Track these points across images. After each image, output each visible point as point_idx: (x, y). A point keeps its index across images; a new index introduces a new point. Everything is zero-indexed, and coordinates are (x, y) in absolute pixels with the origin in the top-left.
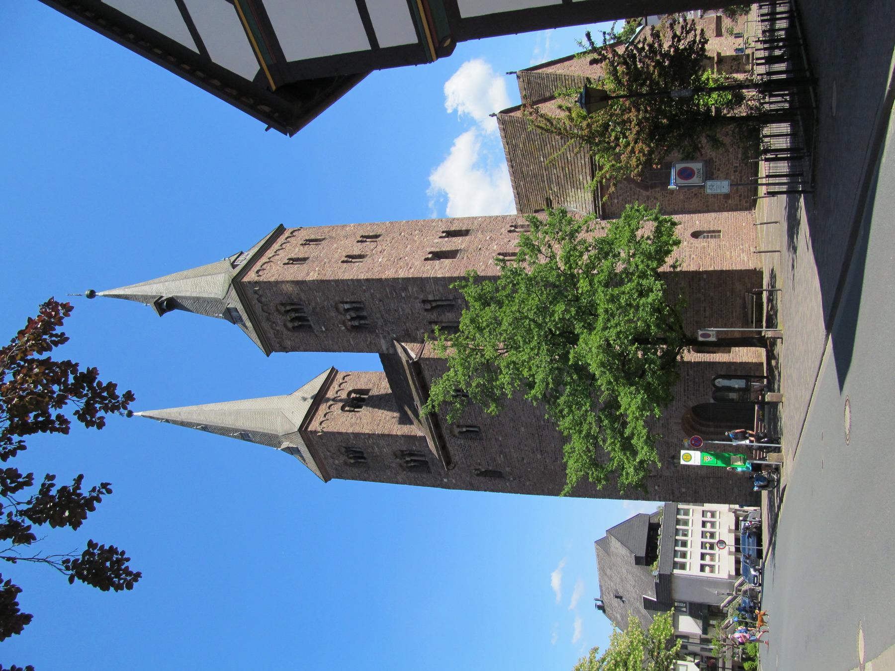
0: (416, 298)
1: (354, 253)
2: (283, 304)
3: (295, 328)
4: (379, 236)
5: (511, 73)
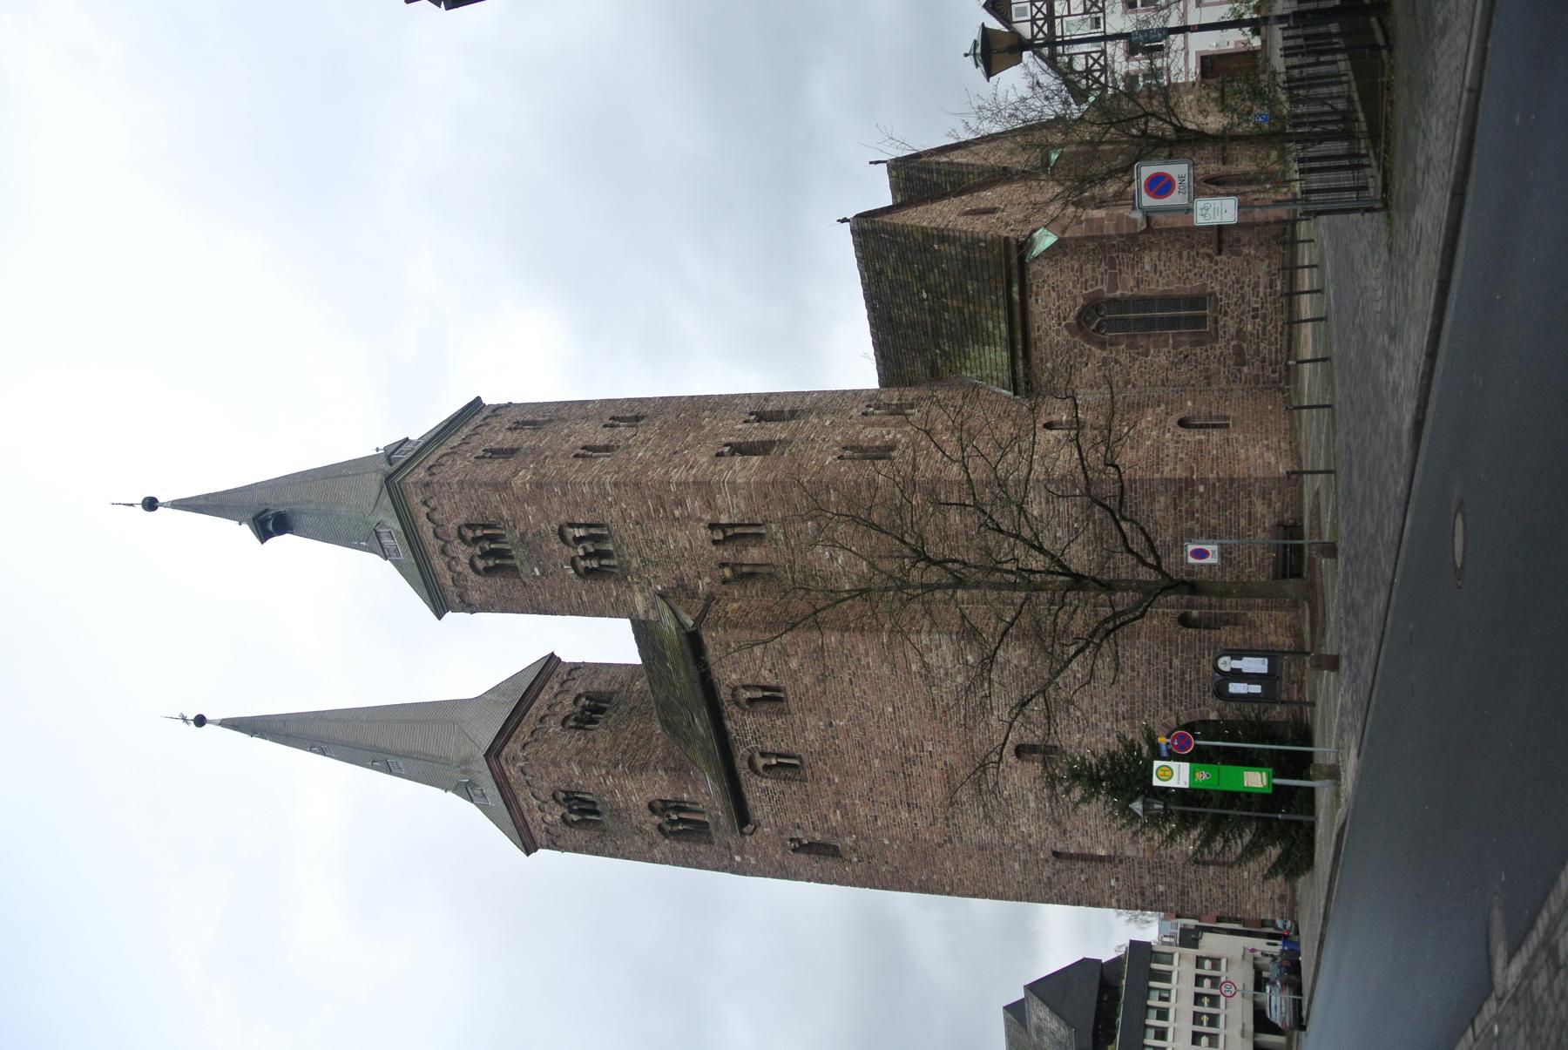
2: (469, 526)
3: (488, 571)
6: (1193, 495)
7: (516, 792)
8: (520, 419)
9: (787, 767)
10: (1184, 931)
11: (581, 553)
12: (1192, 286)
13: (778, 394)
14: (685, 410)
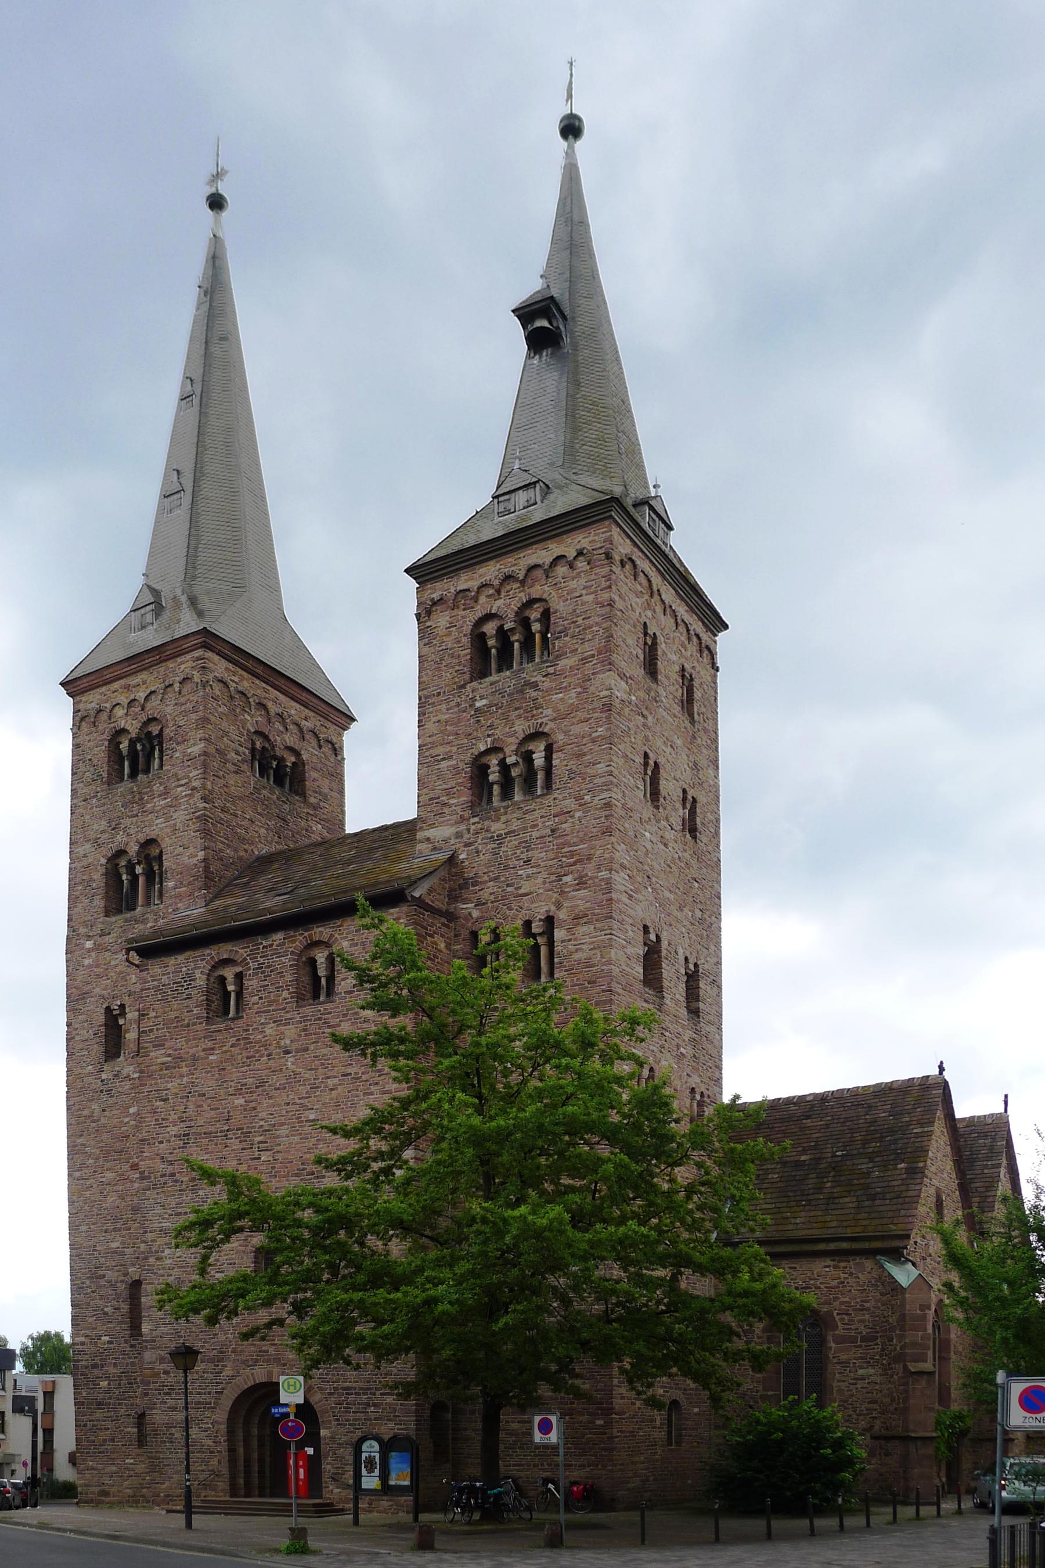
1: (662, 782)
4: (695, 838)
5: (1006, 1103)
6: (591, 1414)
9: (223, 1001)
10: (33, 1399)
11: (510, 760)
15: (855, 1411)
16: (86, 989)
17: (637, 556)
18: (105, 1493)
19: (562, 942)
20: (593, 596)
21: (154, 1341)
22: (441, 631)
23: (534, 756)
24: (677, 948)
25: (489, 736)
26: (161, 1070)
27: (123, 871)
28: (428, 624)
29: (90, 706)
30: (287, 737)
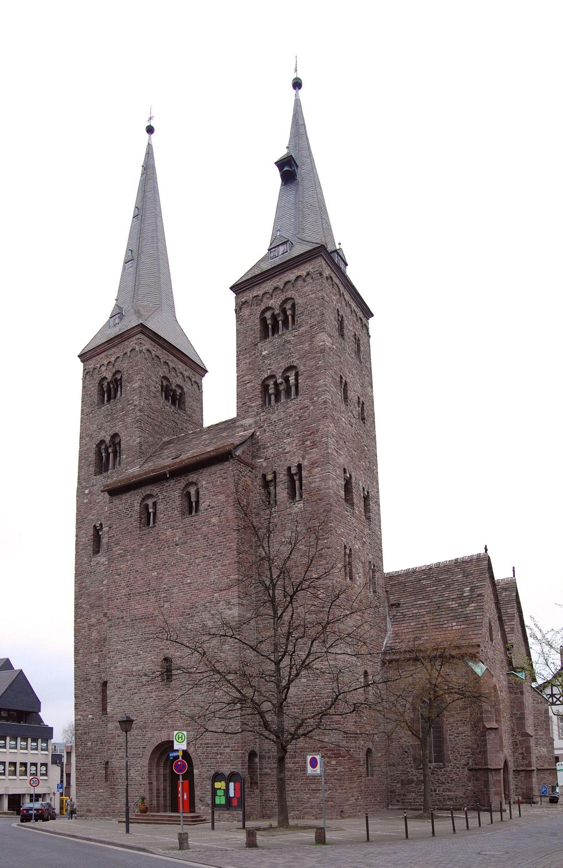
0: (304, 458)
1: (349, 392)
7: (119, 346)
8: (361, 342)
9: (147, 517)
10: (61, 756)
12: (449, 754)
13: (379, 510)
14: (369, 450)
15: (459, 753)
16: (85, 515)
17: (333, 275)
18: (89, 811)
19: (306, 478)
20: (314, 295)
21: (113, 717)
22: (246, 317)
23: (290, 378)
24: (360, 482)
25: (269, 369)
26: (118, 558)
27: (103, 451)
28: (241, 314)
29: (90, 367)
30: (177, 379)
